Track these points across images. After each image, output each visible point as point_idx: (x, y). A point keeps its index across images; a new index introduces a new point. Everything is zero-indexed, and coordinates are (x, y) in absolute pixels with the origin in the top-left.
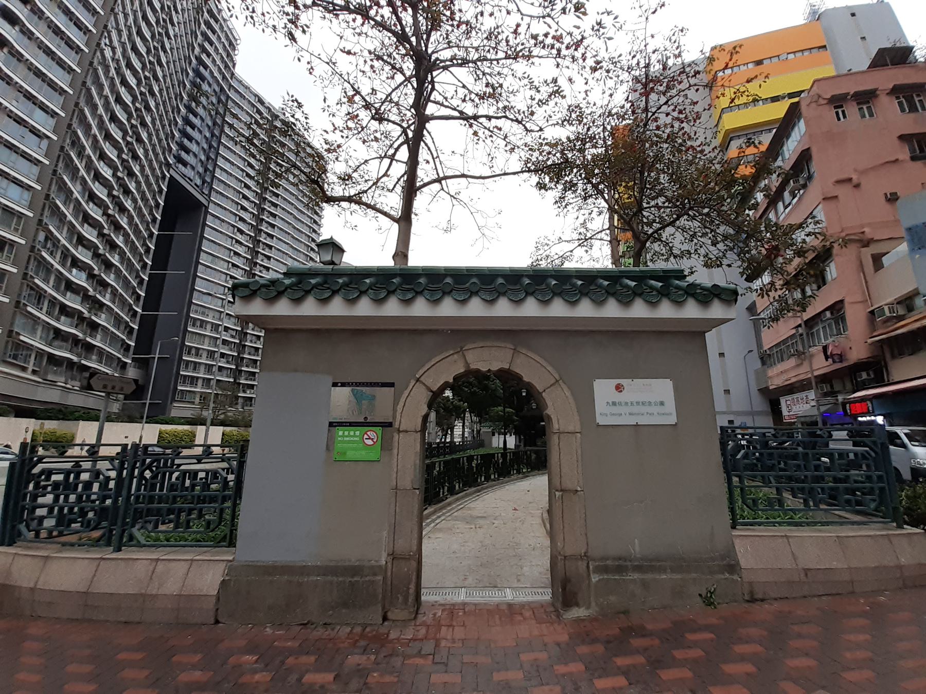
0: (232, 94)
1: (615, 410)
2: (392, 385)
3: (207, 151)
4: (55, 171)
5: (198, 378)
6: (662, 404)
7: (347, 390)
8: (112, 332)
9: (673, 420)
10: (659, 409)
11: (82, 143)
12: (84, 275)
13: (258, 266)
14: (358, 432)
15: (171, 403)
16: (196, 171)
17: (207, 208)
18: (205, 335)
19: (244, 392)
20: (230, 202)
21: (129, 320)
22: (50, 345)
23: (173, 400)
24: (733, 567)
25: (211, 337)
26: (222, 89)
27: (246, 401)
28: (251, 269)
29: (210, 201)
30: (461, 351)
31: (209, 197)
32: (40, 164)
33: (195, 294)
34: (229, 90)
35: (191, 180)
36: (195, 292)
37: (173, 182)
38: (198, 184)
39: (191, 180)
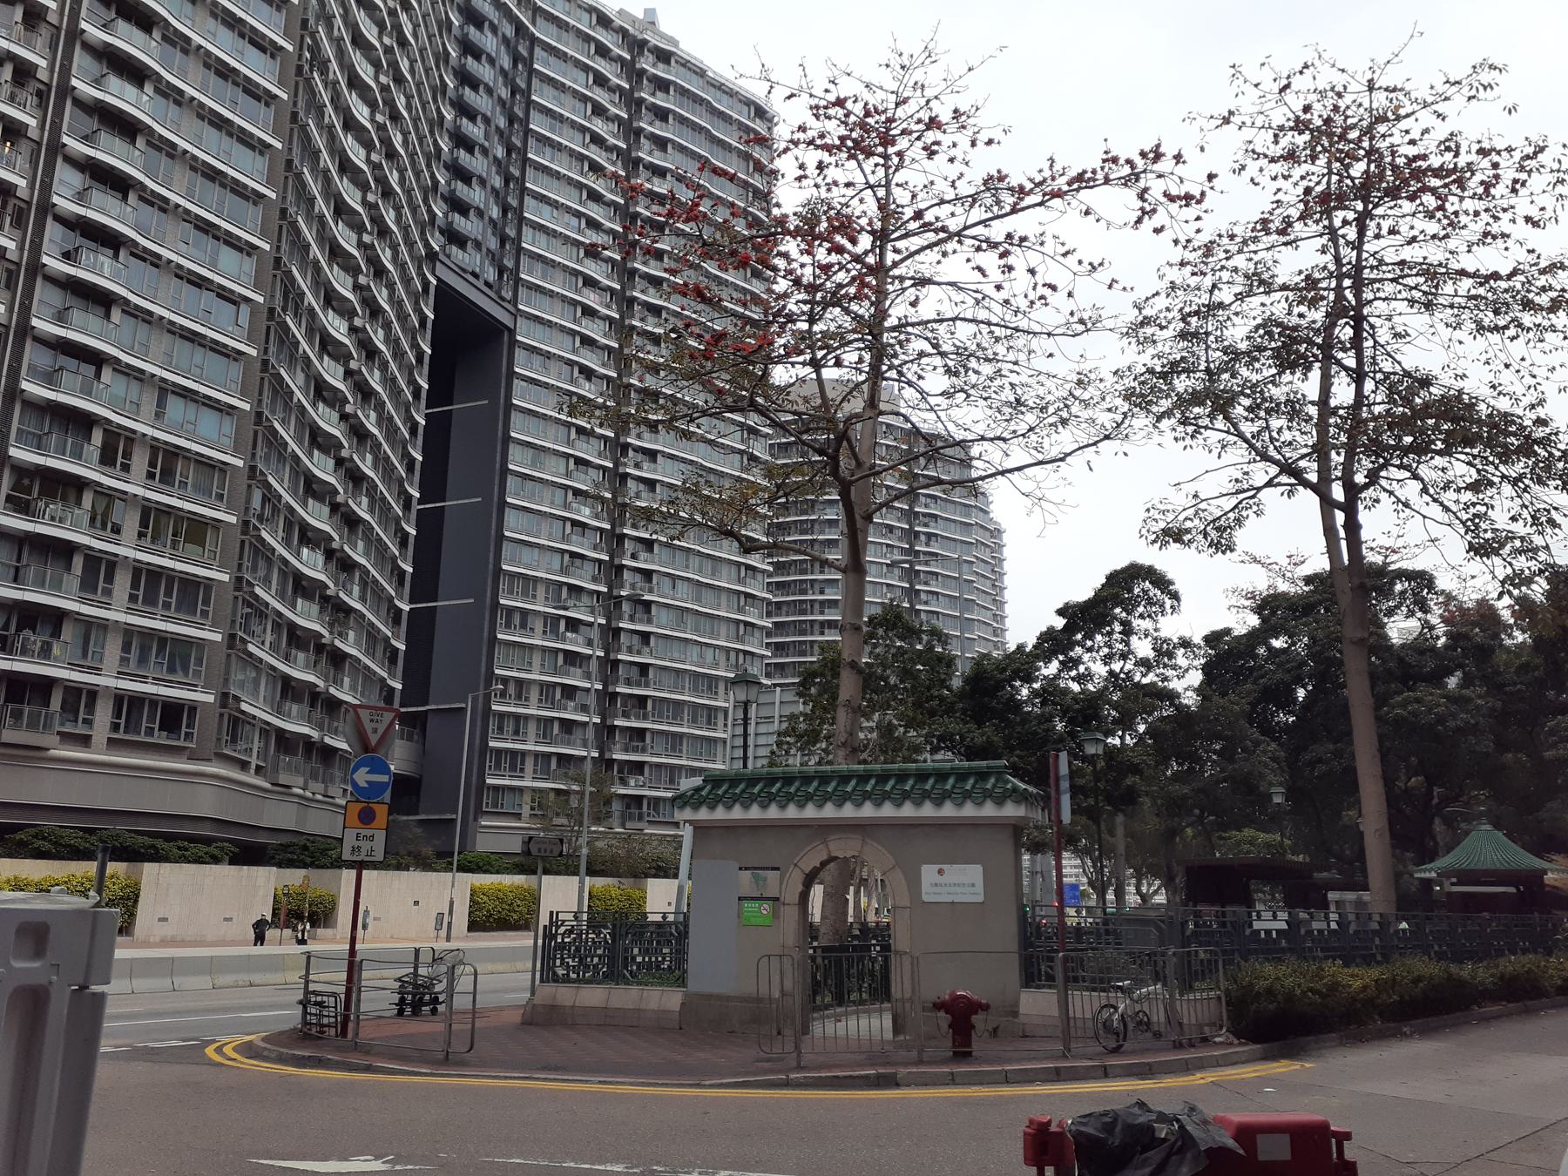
0: (541, 32)
1: (938, 890)
2: (778, 869)
3: (502, 194)
4: (265, 363)
5: (524, 753)
6: (973, 885)
7: (748, 872)
8: (367, 668)
9: (980, 899)
10: (972, 890)
11: (299, 287)
12: (320, 558)
13: (631, 453)
14: (756, 904)
15: (475, 819)
16: (484, 250)
17: (512, 332)
18: (532, 647)
19: (624, 782)
20: (558, 305)
21: (390, 634)
22: (279, 711)
23: (479, 812)
24: (1015, 1014)
25: (544, 649)
26: (520, 28)
27: (628, 807)
28: (616, 464)
29: (516, 314)
30: (825, 842)
31: (515, 305)
32: (243, 357)
33: (506, 548)
34: (534, 24)
35: (476, 275)
36: (505, 544)
37: (444, 289)
38: (491, 279)
39: (476, 275)
